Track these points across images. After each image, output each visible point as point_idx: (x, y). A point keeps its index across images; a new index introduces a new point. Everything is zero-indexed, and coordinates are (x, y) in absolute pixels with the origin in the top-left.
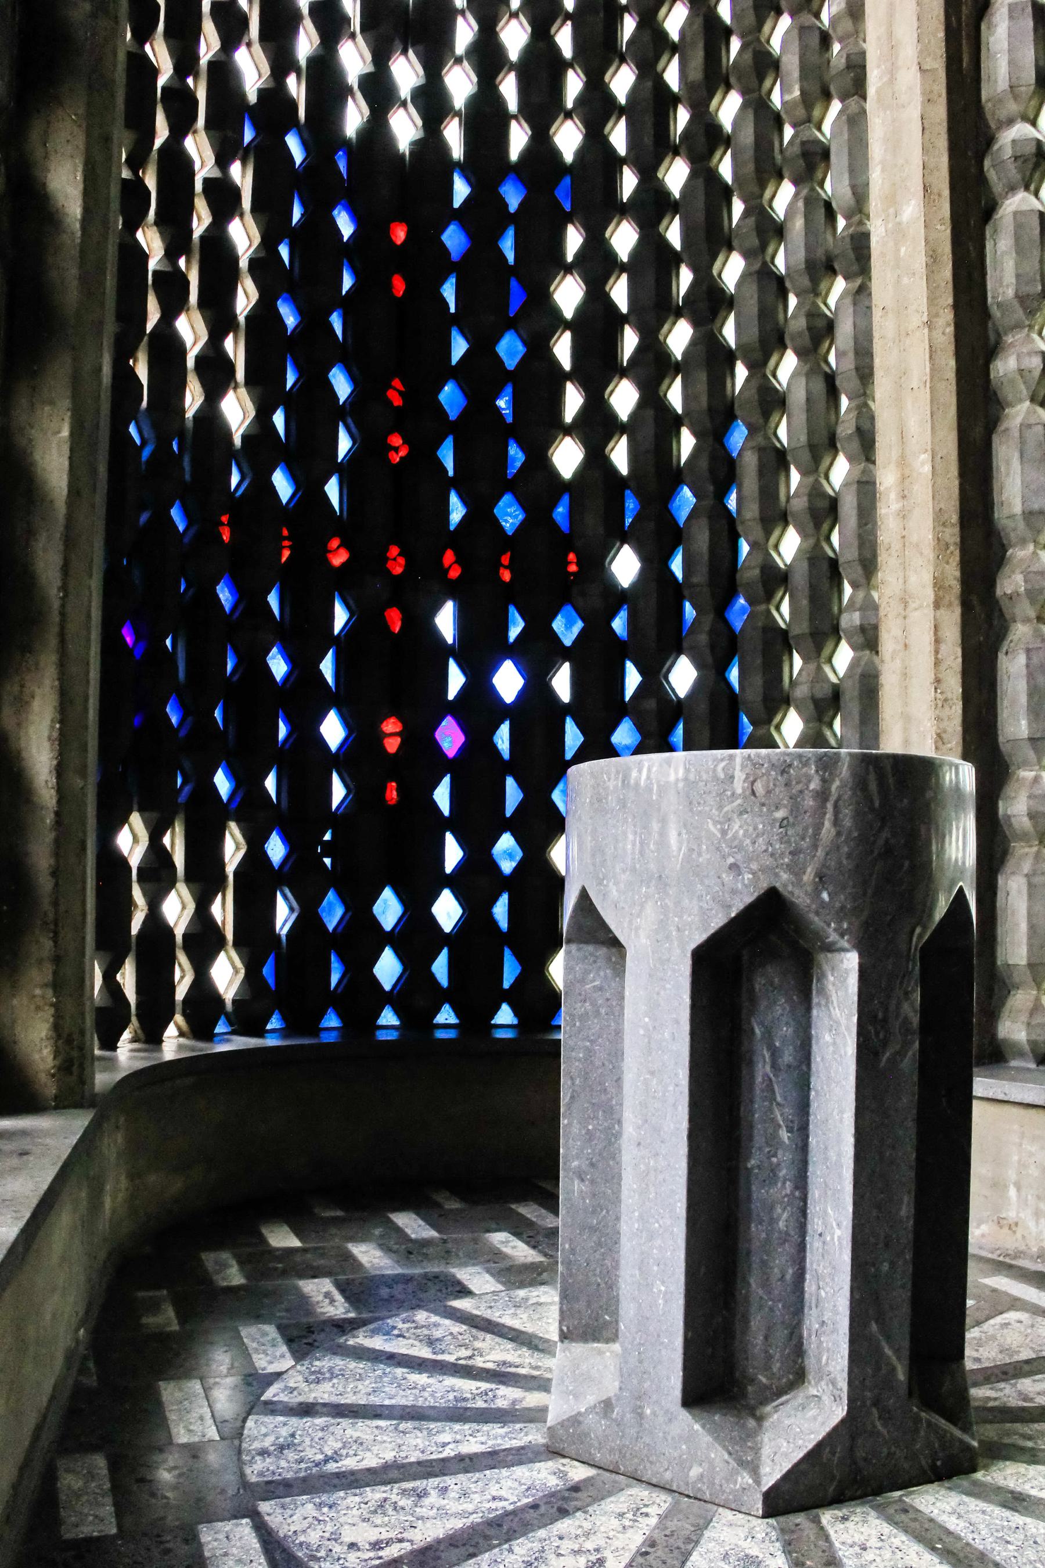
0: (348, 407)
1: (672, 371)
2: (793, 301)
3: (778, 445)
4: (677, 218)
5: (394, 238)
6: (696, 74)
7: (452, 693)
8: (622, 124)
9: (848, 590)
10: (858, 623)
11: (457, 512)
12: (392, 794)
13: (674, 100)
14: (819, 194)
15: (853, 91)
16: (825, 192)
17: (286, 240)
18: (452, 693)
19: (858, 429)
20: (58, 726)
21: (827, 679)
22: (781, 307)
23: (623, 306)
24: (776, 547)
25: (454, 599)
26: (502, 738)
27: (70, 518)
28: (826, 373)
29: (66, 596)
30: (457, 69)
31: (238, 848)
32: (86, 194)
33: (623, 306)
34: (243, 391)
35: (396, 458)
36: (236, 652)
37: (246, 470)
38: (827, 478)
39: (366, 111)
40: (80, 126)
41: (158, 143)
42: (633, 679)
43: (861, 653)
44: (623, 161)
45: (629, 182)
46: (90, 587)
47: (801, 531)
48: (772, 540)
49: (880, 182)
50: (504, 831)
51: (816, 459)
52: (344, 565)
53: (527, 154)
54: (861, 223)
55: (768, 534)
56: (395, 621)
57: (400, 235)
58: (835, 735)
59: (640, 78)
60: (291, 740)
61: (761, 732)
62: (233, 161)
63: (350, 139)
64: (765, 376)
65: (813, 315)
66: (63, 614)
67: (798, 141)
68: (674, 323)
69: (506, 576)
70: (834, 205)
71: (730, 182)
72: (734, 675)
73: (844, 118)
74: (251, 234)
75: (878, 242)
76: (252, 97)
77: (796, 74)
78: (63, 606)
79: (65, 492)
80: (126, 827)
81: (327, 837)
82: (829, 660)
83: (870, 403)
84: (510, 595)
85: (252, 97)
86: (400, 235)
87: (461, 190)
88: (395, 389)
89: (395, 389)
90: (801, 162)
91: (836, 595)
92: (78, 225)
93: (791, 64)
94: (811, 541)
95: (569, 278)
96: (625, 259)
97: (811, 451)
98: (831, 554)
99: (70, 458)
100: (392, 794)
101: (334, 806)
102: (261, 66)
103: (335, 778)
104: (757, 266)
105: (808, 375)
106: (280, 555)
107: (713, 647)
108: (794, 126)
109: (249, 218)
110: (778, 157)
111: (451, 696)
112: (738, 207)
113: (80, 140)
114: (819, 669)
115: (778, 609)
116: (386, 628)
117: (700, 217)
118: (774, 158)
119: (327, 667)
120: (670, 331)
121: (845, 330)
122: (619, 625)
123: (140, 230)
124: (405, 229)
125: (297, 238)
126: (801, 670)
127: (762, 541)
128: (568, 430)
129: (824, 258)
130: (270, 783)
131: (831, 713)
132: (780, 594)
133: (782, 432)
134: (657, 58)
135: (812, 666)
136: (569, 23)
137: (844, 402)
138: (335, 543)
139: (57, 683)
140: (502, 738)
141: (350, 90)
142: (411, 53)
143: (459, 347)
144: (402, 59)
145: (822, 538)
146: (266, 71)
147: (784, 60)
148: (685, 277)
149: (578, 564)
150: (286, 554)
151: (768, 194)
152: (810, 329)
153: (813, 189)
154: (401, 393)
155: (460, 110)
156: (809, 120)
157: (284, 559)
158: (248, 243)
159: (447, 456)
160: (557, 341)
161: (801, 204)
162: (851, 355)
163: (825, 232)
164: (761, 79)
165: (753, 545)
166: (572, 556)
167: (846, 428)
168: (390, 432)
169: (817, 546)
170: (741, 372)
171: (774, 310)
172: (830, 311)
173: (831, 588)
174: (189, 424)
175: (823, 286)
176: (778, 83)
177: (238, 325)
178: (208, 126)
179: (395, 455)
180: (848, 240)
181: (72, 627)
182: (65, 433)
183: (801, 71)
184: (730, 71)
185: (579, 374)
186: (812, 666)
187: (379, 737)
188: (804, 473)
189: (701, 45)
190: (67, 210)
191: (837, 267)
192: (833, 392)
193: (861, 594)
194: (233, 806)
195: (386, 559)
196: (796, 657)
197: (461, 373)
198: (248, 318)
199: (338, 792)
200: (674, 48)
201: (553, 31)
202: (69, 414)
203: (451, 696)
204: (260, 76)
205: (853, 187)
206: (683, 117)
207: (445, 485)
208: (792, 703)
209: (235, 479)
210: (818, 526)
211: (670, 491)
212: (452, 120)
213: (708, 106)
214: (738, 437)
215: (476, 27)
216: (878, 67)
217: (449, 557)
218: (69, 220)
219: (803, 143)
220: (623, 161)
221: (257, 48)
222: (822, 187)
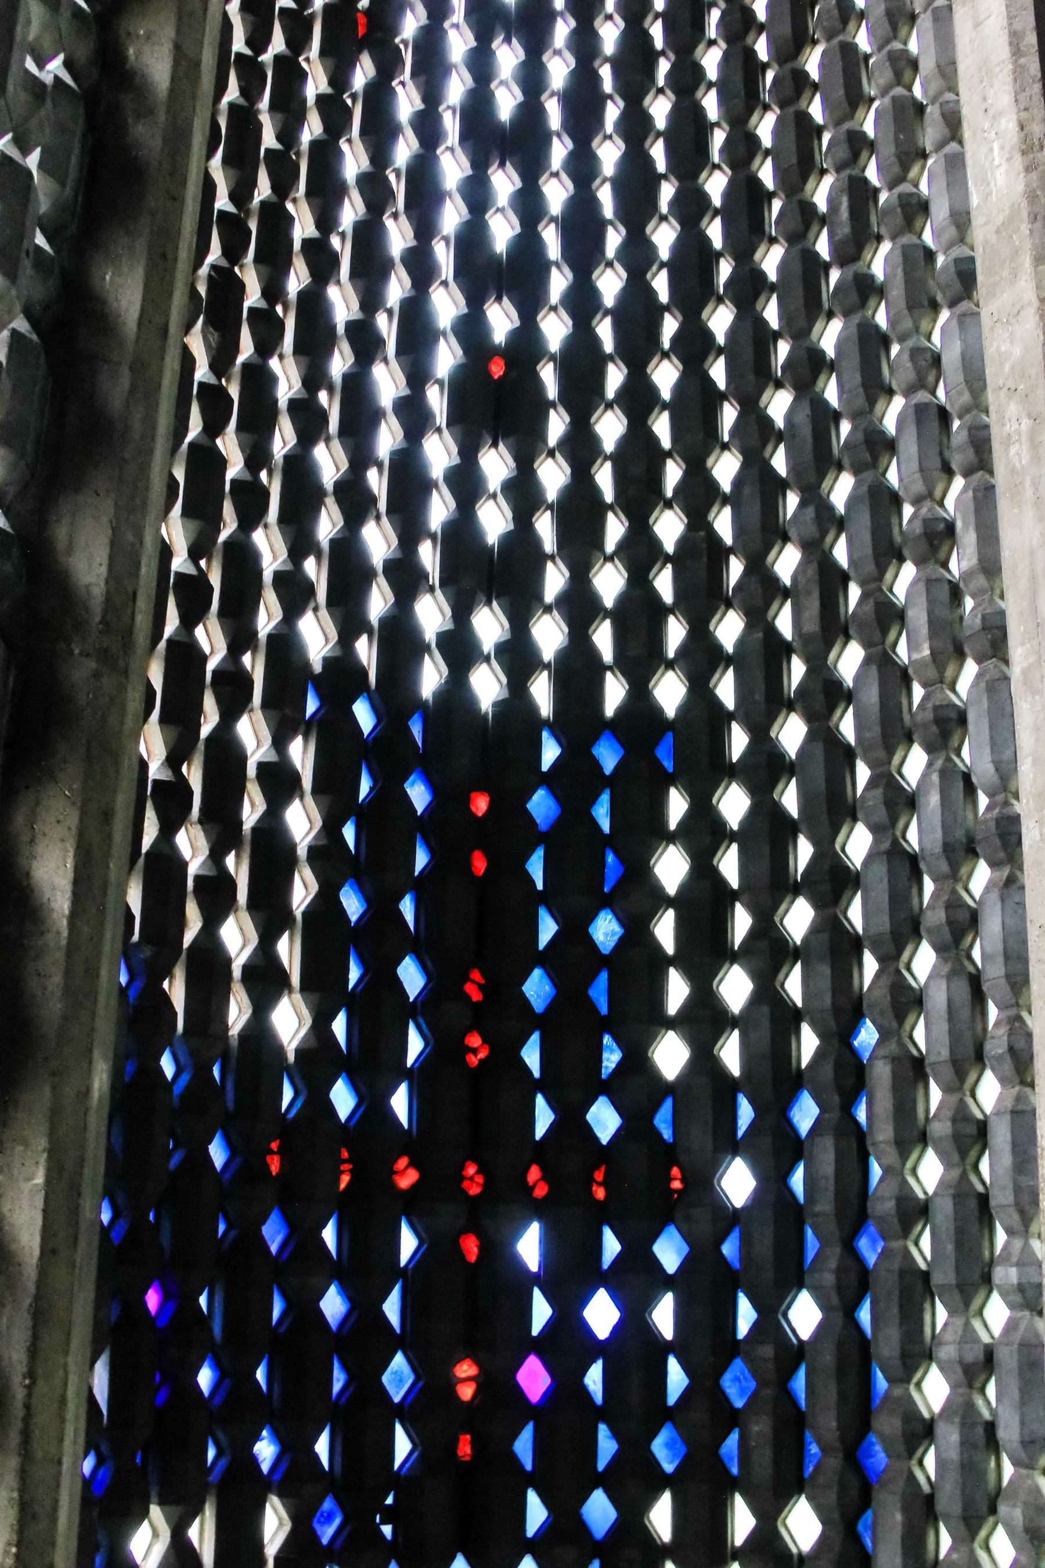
0: (419, 1005)
1: (791, 958)
2: (929, 886)
3: (915, 1052)
4: (794, 782)
5: (473, 809)
6: (812, 625)
7: (537, 1326)
8: (730, 674)
9: (1001, 1237)
10: (1015, 1281)
11: (544, 1118)
12: (465, 1449)
13: (787, 649)
14: (955, 765)
15: (990, 652)
16: (962, 760)
17: (353, 818)
18: (537, 1326)
19: (1011, 1049)
20: (14, 1550)
21: (977, 1340)
22: (915, 891)
23: (734, 881)
24: (914, 1171)
25: (540, 1221)
26: (594, 1378)
27: (40, 1284)
28: (970, 974)
29: (33, 1383)
30: (546, 618)
31: (281, 1524)
32: (77, 882)
33: (734, 881)
34: (297, 997)
35: (474, 1060)
36: (285, 1296)
37: (301, 1086)
38: (973, 1095)
39: (445, 671)
40: (74, 804)
41: (205, 731)
42: (746, 1315)
43: (1020, 1314)
44: (731, 716)
45: (739, 741)
46: (65, 1367)
47: (941, 1155)
48: (909, 1164)
49: (1031, 776)
50: (596, 1487)
51: (961, 1075)
52: (414, 1187)
53: (623, 711)
54: (1006, 804)
55: (904, 1156)
56: (471, 1247)
57: (481, 804)
58: (988, 1403)
59: (749, 627)
60: (347, 1395)
61: (898, 1391)
62: (293, 737)
63: (427, 701)
64: (898, 972)
65: (954, 904)
66: (27, 1406)
67: (930, 705)
68: (793, 902)
69: (600, 1193)
70: (974, 779)
71: (853, 743)
72: (864, 1315)
73: (983, 685)
74: (312, 817)
75: (1031, 846)
76: (317, 667)
77: (924, 631)
78: (29, 1395)
79: (37, 1252)
80: (146, 1523)
81: (389, 1501)
82: (980, 1313)
83: (1024, 1014)
84: (603, 1214)
85: (317, 667)
86: (481, 804)
87: (550, 753)
88: (474, 982)
89: (474, 982)
90: (934, 729)
91: (987, 1236)
92: (65, 922)
93: (918, 617)
94: (956, 1173)
95: (672, 848)
96: (735, 827)
97: (954, 1066)
98: (980, 1188)
99: (44, 1211)
100: (465, 1449)
101: (397, 1464)
102: (328, 631)
103: (399, 1430)
104: (886, 845)
105: (949, 977)
106: (338, 1181)
107: (840, 1288)
108: (924, 685)
109: (309, 799)
110: (907, 718)
111: (536, 1330)
112: (863, 773)
113: (73, 819)
114: (967, 1326)
115: (916, 1244)
116: (461, 1256)
117: (821, 784)
118: (902, 719)
119: (392, 1308)
120: (787, 911)
121: (992, 924)
122: (729, 1249)
123: (183, 830)
124: (488, 799)
125: (365, 817)
126: (946, 1325)
127: (898, 1166)
128: (671, 1024)
129: (964, 840)
130: (322, 1446)
131: (983, 1377)
132: (919, 1227)
133: (920, 1035)
134: (768, 606)
135: (959, 1322)
136: (669, 566)
137: (993, 1012)
138: (403, 1162)
139: (15, 1495)
140: (594, 1378)
141: (427, 648)
142: (495, 604)
143: (547, 929)
144: (485, 610)
145: (969, 1168)
146: (334, 635)
147: (911, 614)
148: (804, 851)
149: (683, 1180)
150: (345, 1179)
151: (896, 760)
152: (950, 922)
153: (949, 760)
154: (481, 987)
155: (550, 663)
156: (930, 496)
157: (343, 1186)
158: (308, 826)
159: (531, 1056)
160: (658, 921)
161: (935, 778)
162: (1000, 959)
163: (964, 810)
164: (885, 631)
165: (887, 1171)
166: (675, 1171)
167: (996, 1045)
168: (468, 1030)
169: (964, 1176)
170: (870, 965)
171: (908, 898)
172: (974, 900)
173: (981, 1231)
174: (234, 1043)
175: (964, 871)
176: (904, 634)
177: (294, 919)
178: (265, 705)
179: (473, 1057)
180: (992, 825)
181: (41, 1419)
182: (39, 1179)
183: (929, 626)
184: (850, 622)
185: (683, 960)
186: (959, 1322)
187: (450, 1385)
188: (946, 1090)
189: (816, 595)
190: (53, 905)
191: (978, 850)
192: (978, 998)
193: (1018, 1244)
194: (277, 1477)
195: (462, 1178)
196: (933, 1086)
197: (550, 958)
198: (305, 914)
199: (402, 1445)
200: (786, 593)
201: (651, 576)
202: (45, 1155)
203: (536, 1330)
204: (327, 641)
205: (997, 765)
206: (797, 669)
207: (530, 1087)
208: (930, 1143)
209: (288, 1094)
210: (963, 1154)
211: (789, 1099)
212: (541, 673)
213: (826, 658)
214: (867, 1036)
215: (567, 574)
216: (1023, 644)
217: (534, 1174)
218: (55, 916)
219: (936, 708)
220: (731, 716)
221: (324, 612)
222: (959, 754)
